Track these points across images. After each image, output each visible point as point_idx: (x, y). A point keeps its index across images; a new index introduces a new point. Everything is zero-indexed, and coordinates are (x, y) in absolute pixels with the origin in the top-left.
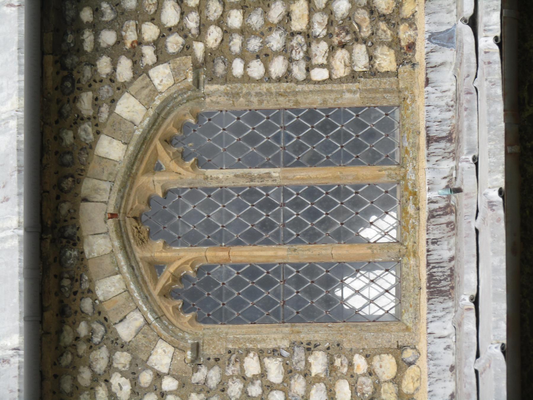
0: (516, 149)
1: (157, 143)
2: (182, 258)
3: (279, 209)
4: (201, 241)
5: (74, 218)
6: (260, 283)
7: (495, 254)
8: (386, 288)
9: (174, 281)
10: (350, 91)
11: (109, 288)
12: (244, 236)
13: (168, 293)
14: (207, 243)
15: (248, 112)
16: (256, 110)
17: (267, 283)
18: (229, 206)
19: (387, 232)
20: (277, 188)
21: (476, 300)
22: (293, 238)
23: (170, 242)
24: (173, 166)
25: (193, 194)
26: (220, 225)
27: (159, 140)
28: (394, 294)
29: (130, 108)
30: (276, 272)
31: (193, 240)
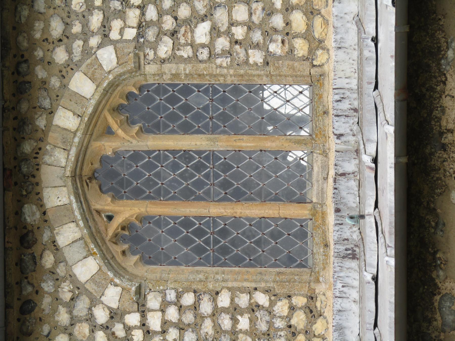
0: (404, 160)
1: (106, 113)
2: (128, 211)
3: (209, 171)
4: (144, 196)
5: (39, 193)
6: (193, 233)
7: (392, 153)
8: (301, 95)
9: (123, 228)
10: (267, 282)
11: (68, 234)
12: (180, 127)
13: (117, 238)
14: (149, 198)
15: (183, 152)
16: (189, 151)
17: (199, 167)
18: (166, 167)
19: (302, 109)
20: (208, 218)
21: (375, 161)
22: (221, 262)
23: (117, 196)
24: (120, 132)
25: (136, 156)
26: (160, 183)
27: (109, 111)
28: (308, 95)
29: (82, 85)
30: (207, 158)
31: (137, 194)
